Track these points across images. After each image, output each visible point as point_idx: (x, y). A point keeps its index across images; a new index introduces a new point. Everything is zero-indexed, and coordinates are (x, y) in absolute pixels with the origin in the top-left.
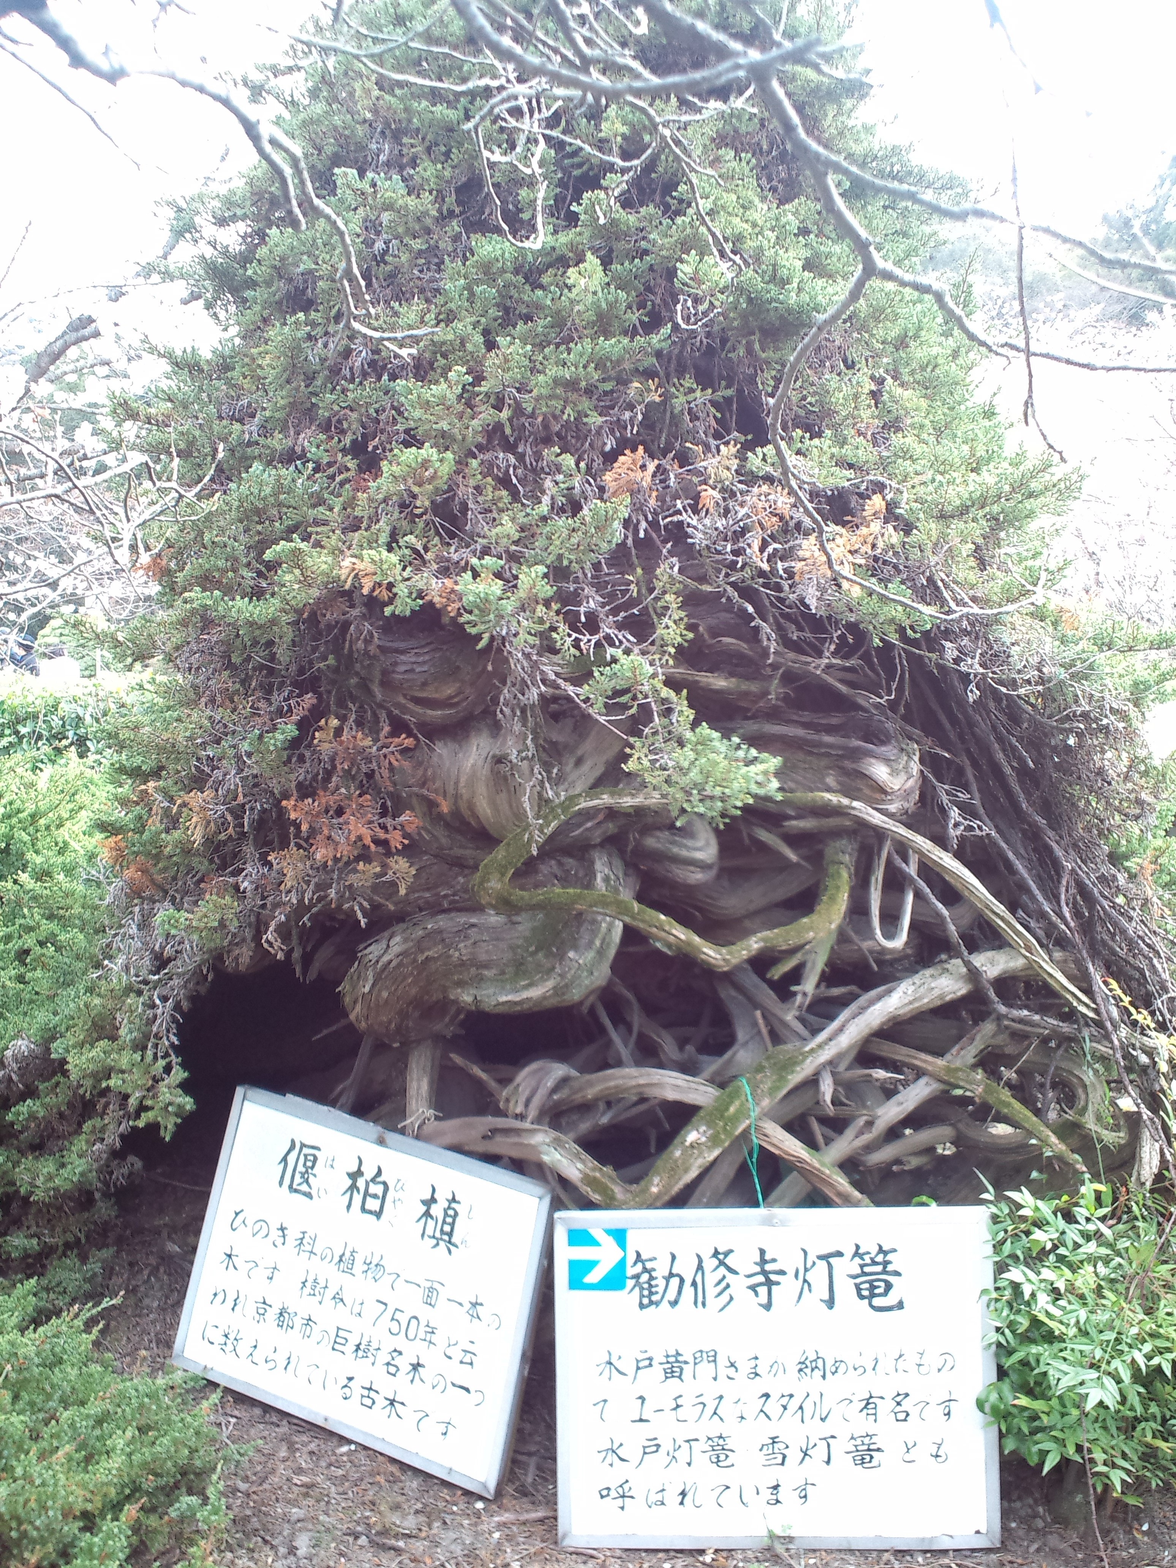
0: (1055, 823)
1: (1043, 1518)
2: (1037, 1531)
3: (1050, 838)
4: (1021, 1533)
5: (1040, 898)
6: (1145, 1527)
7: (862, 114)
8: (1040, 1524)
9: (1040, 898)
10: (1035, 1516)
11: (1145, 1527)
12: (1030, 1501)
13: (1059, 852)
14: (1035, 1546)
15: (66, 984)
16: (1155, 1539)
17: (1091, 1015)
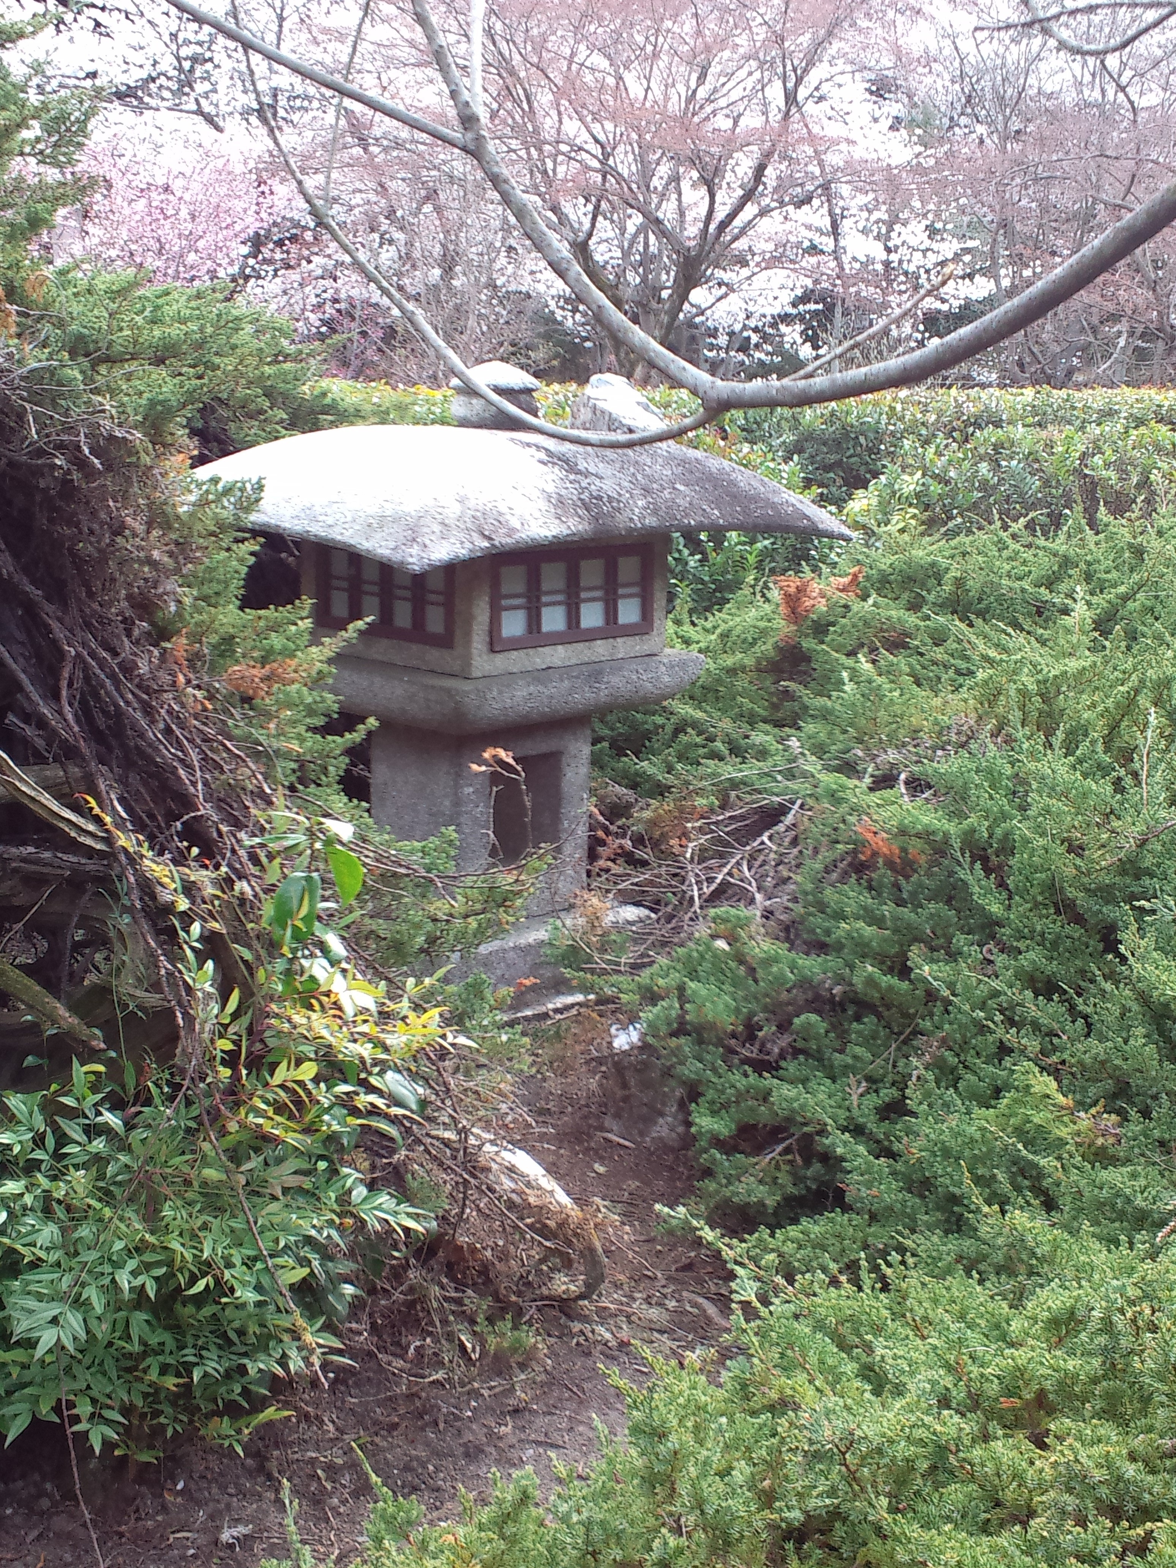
0: (58, 593)
1: (50, 1496)
2: (42, 1513)
3: (49, 611)
4: (18, 1520)
5: (35, 697)
6: (180, 1486)
7: (551, 488)
8: (45, 1503)
9: (35, 697)
10: (42, 1494)
11: (180, 1486)
12: (37, 1477)
13: (59, 632)
14: (36, 1533)
15: (1111, 1411)
16: (191, 1498)
17: (99, 846)
